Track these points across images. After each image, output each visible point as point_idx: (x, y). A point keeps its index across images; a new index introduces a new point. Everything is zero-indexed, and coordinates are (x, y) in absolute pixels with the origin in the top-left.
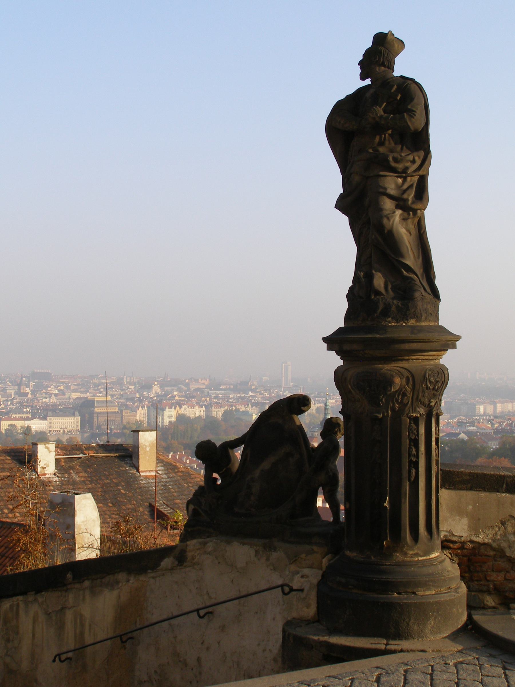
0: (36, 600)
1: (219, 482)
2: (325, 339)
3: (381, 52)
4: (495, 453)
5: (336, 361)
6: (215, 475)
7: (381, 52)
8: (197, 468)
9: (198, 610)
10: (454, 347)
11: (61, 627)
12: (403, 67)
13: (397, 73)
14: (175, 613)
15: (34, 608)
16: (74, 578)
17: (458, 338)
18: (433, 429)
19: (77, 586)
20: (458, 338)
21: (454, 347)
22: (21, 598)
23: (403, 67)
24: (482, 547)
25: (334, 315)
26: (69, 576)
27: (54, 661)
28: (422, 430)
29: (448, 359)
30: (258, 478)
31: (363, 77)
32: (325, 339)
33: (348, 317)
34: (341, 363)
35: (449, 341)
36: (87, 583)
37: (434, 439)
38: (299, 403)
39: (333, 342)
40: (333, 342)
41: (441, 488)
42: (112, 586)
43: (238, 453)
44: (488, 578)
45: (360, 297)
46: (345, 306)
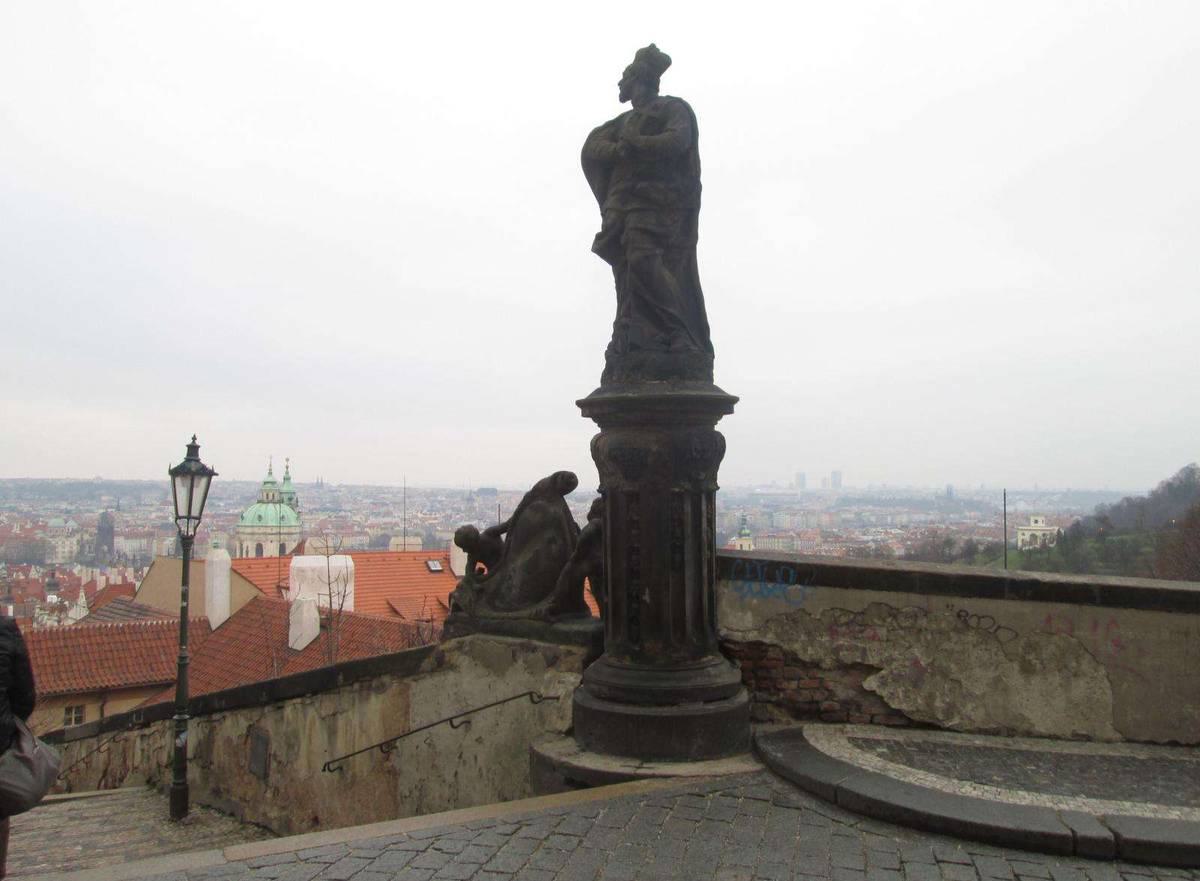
0: (312, 703)
1: (486, 572)
2: (579, 403)
3: (648, 66)
4: (900, 558)
5: (592, 429)
6: (480, 565)
7: (648, 66)
8: (460, 560)
9: (450, 720)
10: (731, 411)
11: (332, 732)
12: (669, 85)
13: (663, 92)
14: (435, 721)
15: (311, 712)
16: (345, 679)
17: (735, 400)
18: (704, 508)
19: (348, 688)
20: (735, 400)
21: (731, 411)
22: (299, 700)
23: (669, 85)
24: (771, 649)
25: (589, 378)
26: (341, 677)
27: (324, 770)
28: (688, 508)
29: (724, 426)
30: (521, 564)
31: (623, 99)
32: (579, 403)
33: (607, 376)
34: (598, 430)
35: (726, 404)
36: (356, 686)
37: (704, 520)
38: (564, 482)
39: (588, 407)
40: (588, 407)
41: (719, 578)
42: (381, 689)
43: (504, 536)
44: (779, 687)
45: (622, 356)
46: (601, 364)
